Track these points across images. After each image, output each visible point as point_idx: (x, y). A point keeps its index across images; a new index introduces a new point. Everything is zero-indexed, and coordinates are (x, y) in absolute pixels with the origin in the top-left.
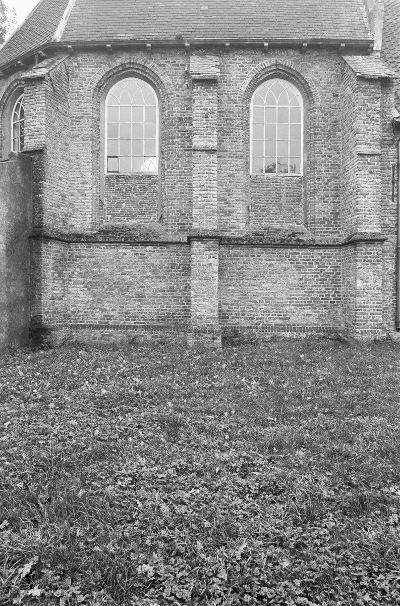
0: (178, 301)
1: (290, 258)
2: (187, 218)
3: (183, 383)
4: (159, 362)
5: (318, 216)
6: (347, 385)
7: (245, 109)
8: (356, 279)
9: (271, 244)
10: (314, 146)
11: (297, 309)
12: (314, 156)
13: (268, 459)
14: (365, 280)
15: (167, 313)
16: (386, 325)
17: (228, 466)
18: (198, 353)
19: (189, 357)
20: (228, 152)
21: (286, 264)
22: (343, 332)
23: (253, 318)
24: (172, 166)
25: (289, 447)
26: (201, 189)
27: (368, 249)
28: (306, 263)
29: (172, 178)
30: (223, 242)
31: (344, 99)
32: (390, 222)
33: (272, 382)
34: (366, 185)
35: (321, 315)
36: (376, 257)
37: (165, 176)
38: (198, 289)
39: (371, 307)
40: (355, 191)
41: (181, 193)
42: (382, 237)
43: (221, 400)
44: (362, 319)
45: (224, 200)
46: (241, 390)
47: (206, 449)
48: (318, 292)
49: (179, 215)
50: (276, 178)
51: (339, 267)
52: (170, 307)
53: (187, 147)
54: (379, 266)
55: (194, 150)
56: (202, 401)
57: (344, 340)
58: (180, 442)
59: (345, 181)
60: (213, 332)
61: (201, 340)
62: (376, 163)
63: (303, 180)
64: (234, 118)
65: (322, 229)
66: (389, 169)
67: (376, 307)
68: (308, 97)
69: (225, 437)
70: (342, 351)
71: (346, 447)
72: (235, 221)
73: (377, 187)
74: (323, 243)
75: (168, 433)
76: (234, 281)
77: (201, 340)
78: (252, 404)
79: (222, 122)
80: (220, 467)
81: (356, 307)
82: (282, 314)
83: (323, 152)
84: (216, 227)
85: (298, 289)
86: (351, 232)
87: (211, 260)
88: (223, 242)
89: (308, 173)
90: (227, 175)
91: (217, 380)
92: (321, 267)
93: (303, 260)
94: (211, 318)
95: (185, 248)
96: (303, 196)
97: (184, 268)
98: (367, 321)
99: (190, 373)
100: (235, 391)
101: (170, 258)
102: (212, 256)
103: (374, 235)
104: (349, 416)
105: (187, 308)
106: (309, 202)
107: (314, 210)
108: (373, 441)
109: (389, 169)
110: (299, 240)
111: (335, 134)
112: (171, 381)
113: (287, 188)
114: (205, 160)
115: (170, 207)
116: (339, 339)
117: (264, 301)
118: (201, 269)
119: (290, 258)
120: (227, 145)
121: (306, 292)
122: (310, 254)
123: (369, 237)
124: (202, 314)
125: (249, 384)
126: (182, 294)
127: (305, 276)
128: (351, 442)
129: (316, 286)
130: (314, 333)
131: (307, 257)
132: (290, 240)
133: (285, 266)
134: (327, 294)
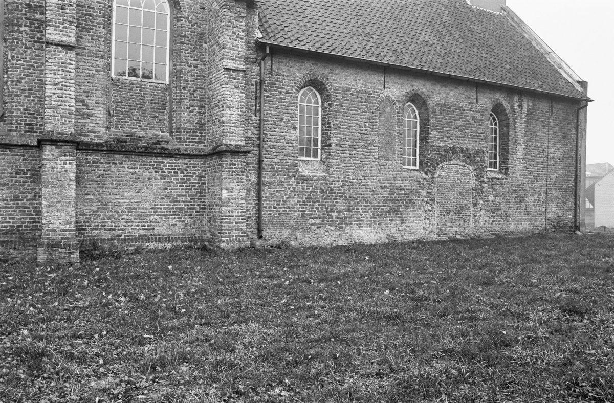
0: (25, 211)
1: (155, 166)
2: (36, 118)
3: (39, 306)
4: (4, 283)
5: (184, 126)
6: (219, 294)
7: (107, 6)
8: (221, 189)
9: (135, 152)
10: (180, 55)
11: (161, 219)
12: (181, 65)
13: (151, 380)
14: (230, 190)
15: (10, 226)
16: (249, 233)
17: (109, 394)
18: (52, 271)
19: (43, 275)
20: (87, 51)
21: (150, 172)
22: (208, 241)
23: (114, 230)
24: (18, 57)
25: (171, 363)
26: (55, 87)
27: (233, 160)
28: (171, 172)
29: (17, 71)
30: (80, 147)
31: (211, 13)
32: (253, 135)
33: (142, 296)
34: (231, 99)
35: (186, 225)
36: (241, 168)
37: (8, 68)
38: (51, 198)
39: (236, 216)
40: (220, 103)
41: (29, 90)
42: (245, 149)
43: (88, 321)
44: (227, 228)
45: (82, 101)
46: (109, 309)
47: (79, 379)
48: (184, 202)
49: (27, 115)
50: (139, 83)
51: (204, 177)
52: (14, 219)
53: (38, 38)
54: (243, 177)
55: (48, 44)
56: (66, 325)
57: (210, 249)
58: (45, 375)
59: (211, 93)
60: (69, 245)
61: (55, 255)
62: (241, 79)
63: (168, 88)
64: (95, 14)
65: (187, 138)
66: (253, 85)
67: (241, 216)
68: (175, 5)
69: (98, 362)
70: (210, 260)
71: (229, 357)
72: (94, 125)
73: (241, 102)
74: (189, 152)
75: (29, 366)
76: (93, 190)
77: (55, 255)
78: (124, 323)
79: (80, 17)
80: (99, 397)
81: (221, 216)
82: (146, 225)
83: (190, 62)
84: (73, 131)
85: (163, 199)
86: (217, 143)
87: (67, 166)
88: (80, 147)
89: (173, 81)
90: (86, 75)
91: (80, 299)
92: (187, 176)
93: (169, 169)
94: (66, 230)
95: (34, 152)
96: (168, 104)
97: (32, 175)
98: (232, 230)
99: (46, 294)
100: (103, 310)
101: (14, 163)
102: (68, 162)
103: (239, 146)
104: (226, 324)
105: (37, 220)
106: (175, 111)
107: (180, 119)
108: (252, 347)
109: (253, 85)
110: (163, 149)
111: (201, 45)
112: (23, 305)
113: (151, 95)
114: (61, 56)
115: (14, 104)
116: (204, 248)
117: (127, 211)
118: (55, 177)
119: (155, 166)
120: (86, 42)
121: (170, 202)
122: (175, 163)
123: (233, 149)
124: (55, 226)
125: (117, 301)
126: (30, 204)
127: (170, 186)
128: (232, 351)
129: (181, 196)
130: (179, 243)
131: (172, 166)
132: (155, 149)
133: (149, 174)
134: (192, 203)
